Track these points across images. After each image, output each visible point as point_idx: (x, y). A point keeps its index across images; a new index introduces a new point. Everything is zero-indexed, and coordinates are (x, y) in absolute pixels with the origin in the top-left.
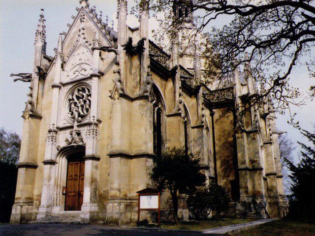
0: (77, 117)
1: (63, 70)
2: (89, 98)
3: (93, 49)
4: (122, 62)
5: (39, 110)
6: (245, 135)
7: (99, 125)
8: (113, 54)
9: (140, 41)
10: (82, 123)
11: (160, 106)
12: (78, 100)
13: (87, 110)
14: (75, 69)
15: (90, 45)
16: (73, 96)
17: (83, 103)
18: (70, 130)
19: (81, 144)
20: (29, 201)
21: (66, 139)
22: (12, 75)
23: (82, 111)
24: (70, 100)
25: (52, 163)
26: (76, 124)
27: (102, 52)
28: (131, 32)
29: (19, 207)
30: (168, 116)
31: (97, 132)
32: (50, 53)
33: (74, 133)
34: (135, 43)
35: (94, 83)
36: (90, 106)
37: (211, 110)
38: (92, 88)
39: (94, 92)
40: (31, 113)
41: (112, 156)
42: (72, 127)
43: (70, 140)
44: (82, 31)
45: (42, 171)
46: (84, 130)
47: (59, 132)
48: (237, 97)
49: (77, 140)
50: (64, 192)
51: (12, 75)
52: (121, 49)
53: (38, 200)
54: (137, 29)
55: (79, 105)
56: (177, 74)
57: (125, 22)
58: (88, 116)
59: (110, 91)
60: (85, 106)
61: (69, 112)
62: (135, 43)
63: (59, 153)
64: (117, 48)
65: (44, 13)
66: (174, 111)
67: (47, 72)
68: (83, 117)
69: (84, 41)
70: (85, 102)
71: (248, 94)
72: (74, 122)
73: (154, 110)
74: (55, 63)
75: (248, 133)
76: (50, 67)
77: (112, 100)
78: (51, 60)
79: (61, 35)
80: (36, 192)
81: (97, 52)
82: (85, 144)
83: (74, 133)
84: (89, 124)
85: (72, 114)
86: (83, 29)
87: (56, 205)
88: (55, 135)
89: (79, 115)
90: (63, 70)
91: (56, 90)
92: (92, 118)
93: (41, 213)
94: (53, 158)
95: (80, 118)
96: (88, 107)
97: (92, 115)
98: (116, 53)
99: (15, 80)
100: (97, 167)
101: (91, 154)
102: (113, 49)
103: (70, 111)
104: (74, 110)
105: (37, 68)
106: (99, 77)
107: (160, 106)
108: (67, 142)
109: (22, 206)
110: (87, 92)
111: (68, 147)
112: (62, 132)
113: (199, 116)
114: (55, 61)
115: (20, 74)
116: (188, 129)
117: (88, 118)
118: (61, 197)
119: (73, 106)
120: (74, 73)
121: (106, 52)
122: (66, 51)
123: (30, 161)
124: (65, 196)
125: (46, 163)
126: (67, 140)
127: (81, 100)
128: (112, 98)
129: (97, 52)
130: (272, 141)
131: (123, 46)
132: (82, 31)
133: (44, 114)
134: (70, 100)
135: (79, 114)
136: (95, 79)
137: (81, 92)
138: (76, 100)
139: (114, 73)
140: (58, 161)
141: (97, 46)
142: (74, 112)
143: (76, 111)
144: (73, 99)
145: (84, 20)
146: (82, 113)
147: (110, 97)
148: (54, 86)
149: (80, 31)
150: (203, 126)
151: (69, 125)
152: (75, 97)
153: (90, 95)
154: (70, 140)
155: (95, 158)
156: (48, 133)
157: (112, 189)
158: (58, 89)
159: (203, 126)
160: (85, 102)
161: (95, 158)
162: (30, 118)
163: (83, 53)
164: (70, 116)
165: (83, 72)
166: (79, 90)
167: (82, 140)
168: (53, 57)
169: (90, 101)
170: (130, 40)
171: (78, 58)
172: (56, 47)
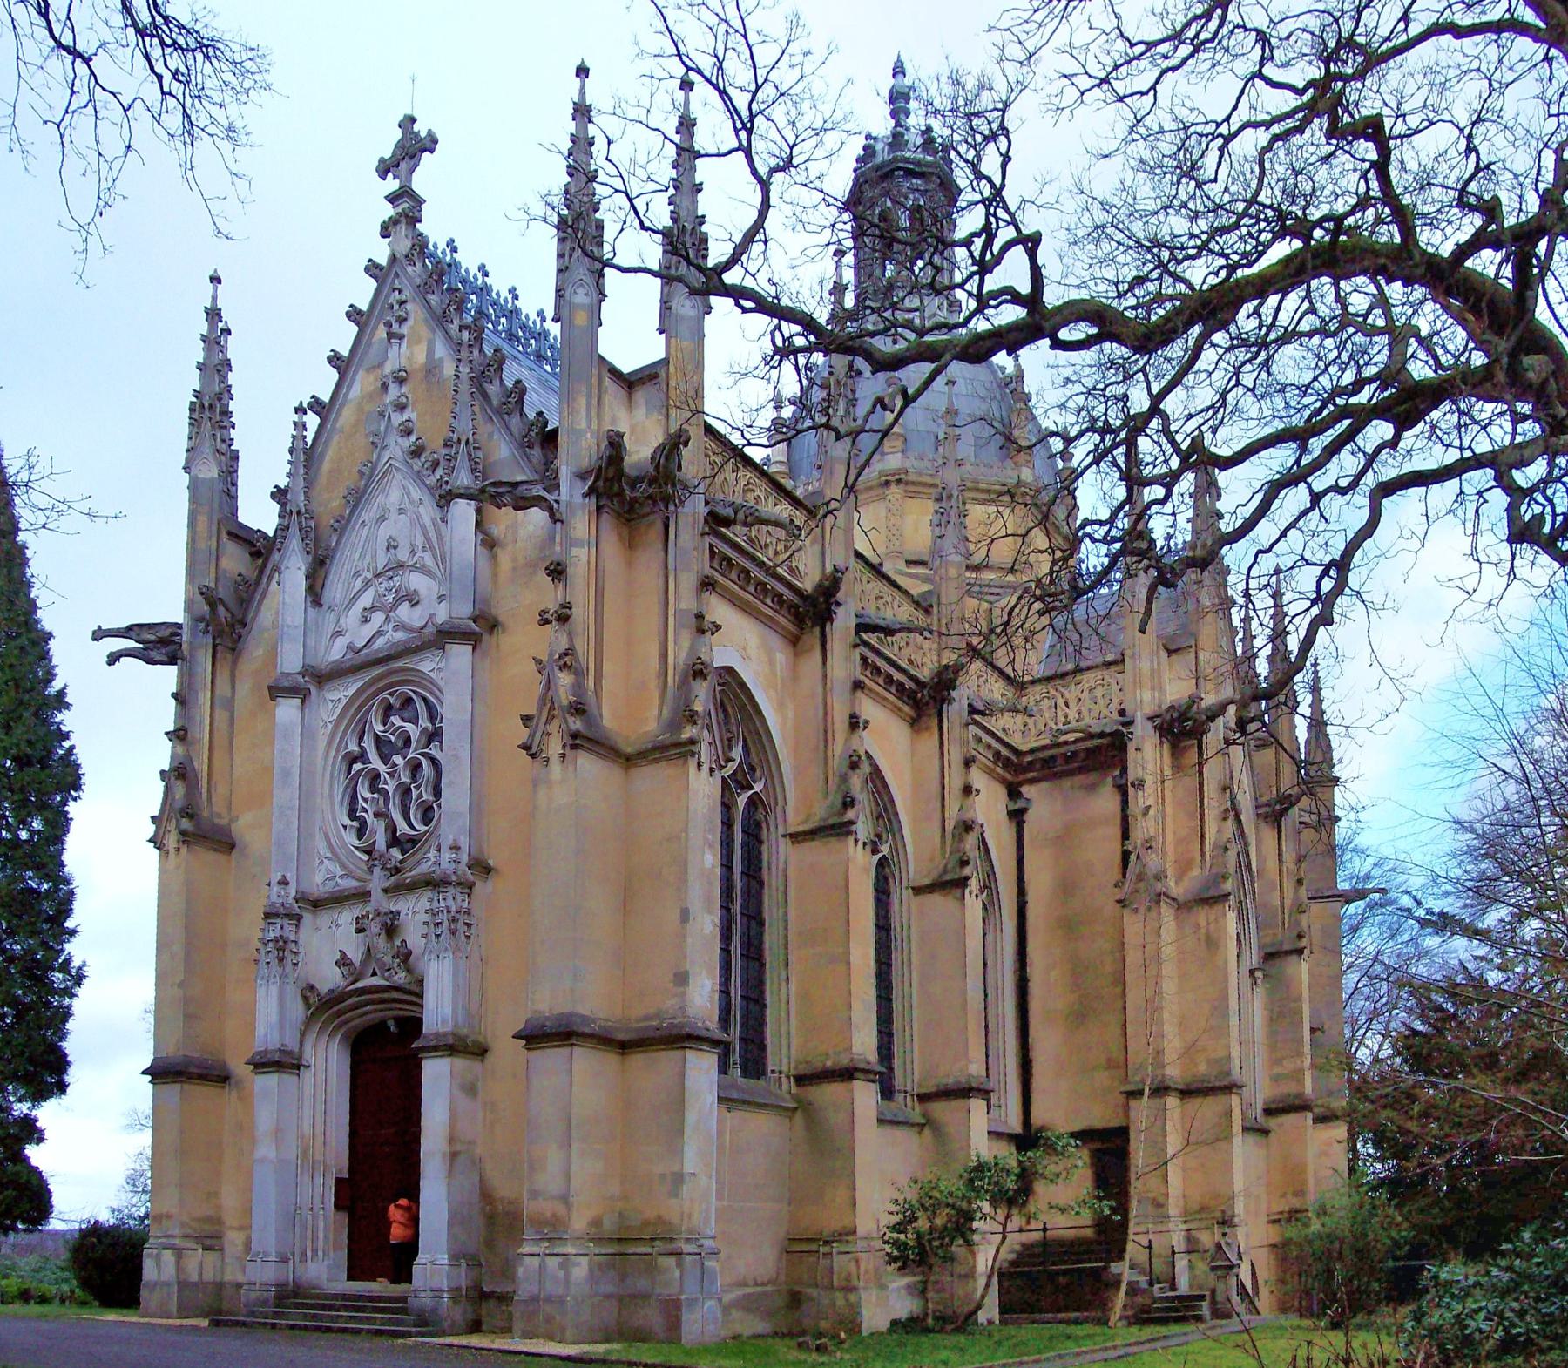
0: (381, 841)
1: (317, 603)
2: (433, 750)
3: (445, 498)
4: (580, 560)
5: (214, 808)
6: (1167, 913)
7: (479, 885)
8: (537, 515)
9: (661, 447)
10: (409, 876)
11: (758, 787)
12: (385, 759)
13: (427, 814)
14: (366, 600)
15: (436, 464)
16: (361, 739)
17: (405, 779)
18: (357, 911)
19: (401, 978)
20: (209, 1229)
21: (338, 956)
22: (99, 635)
25: (284, 1063)
26: (377, 882)
27: (490, 509)
28: (622, 393)
29: (168, 1256)
30: (796, 837)
31: (469, 925)
32: (259, 514)
34: (640, 451)
36: (437, 793)
37: (1013, 792)
38: (447, 699)
39: (455, 710)
40: (186, 824)
41: (536, 1036)
42: (363, 895)
43: (356, 956)
44: (394, 391)
45: (246, 1099)
46: (414, 911)
47: (307, 917)
48: (1139, 718)
49: (388, 959)
51: (99, 635)
52: (570, 491)
53: (241, 1228)
55: (390, 787)
56: (840, 611)
59: (526, 719)
60: (415, 794)
61: (347, 821)
62: (640, 451)
63: (309, 1022)
64: (554, 486)
66: (820, 812)
67: (245, 615)
69: (407, 443)
70: (415, 768)
71: (1194, 700)
72: (370, 870)
73: (727, 807)
74: (277, 569)
75: (1182, 907)
76: (258, 582)
77: (538, 764)
78: (259, 548)
80: (230, 1200)
81: (464, 511)
82: (421, 982)
84: (434, 883)
86: (401, 381)
87: (315, 1252)
88: (292, 937)
89: (394, 840)
90: (317, 603)
91: (287, 710)
92: (447, 855)
94: (292, 1043)
95: (396, 853)
97: (447, 841)
98: (554, 518)
99: (113, 659)
100: (471, 1090)
101: (448, 1028)
102: (537, 491)
103: (352, 814)
105: (199, 598)
106: (470, 638)
107: (758, 787)
108: (346, 970)
109: (178, 1252)
110: (424, 722)
112: (325, 918)
113: (949, 826)
114: (276, 556)
115: (130, 628)
116: (895, 898)
118: (331, 1220)
119: (364, 791)
120: (366, 620)
121: (507, 512)
122: (330, 502)
123: (196, 1055)
125: (264, 1064)
126: (344, 962)
127: (397, 759)
128: (533, 756)
129: (464, 511)
130: (1304, 942)
131: (582, 476)
133: (244, 826)
135: (391, 828)
136: (460, 654)
137: (396, 720)
138: (376, 763)
139: (545, 622)
140: (308, 1055)
141: (463, 479)
142: (370, 819)
143: (377, 815)
144: (362, 757)
145: (405, 330)
146: (402, 827)
147: (526, 747)
148: (277, 691)
149: (385, 387)
151: (349, 884)
152: (369, 744)
153: (434, 736)
154: (356, 956)
155: (455, 1046)
156: (262, 924)
157: (534, 1194)
160: (415, 768)
161: (455, 1046)
162: (184, 849)
164: (351, 839)
165: (404, 611)
166: (388, 711)
169: (434, 762)
170: (615, 444)
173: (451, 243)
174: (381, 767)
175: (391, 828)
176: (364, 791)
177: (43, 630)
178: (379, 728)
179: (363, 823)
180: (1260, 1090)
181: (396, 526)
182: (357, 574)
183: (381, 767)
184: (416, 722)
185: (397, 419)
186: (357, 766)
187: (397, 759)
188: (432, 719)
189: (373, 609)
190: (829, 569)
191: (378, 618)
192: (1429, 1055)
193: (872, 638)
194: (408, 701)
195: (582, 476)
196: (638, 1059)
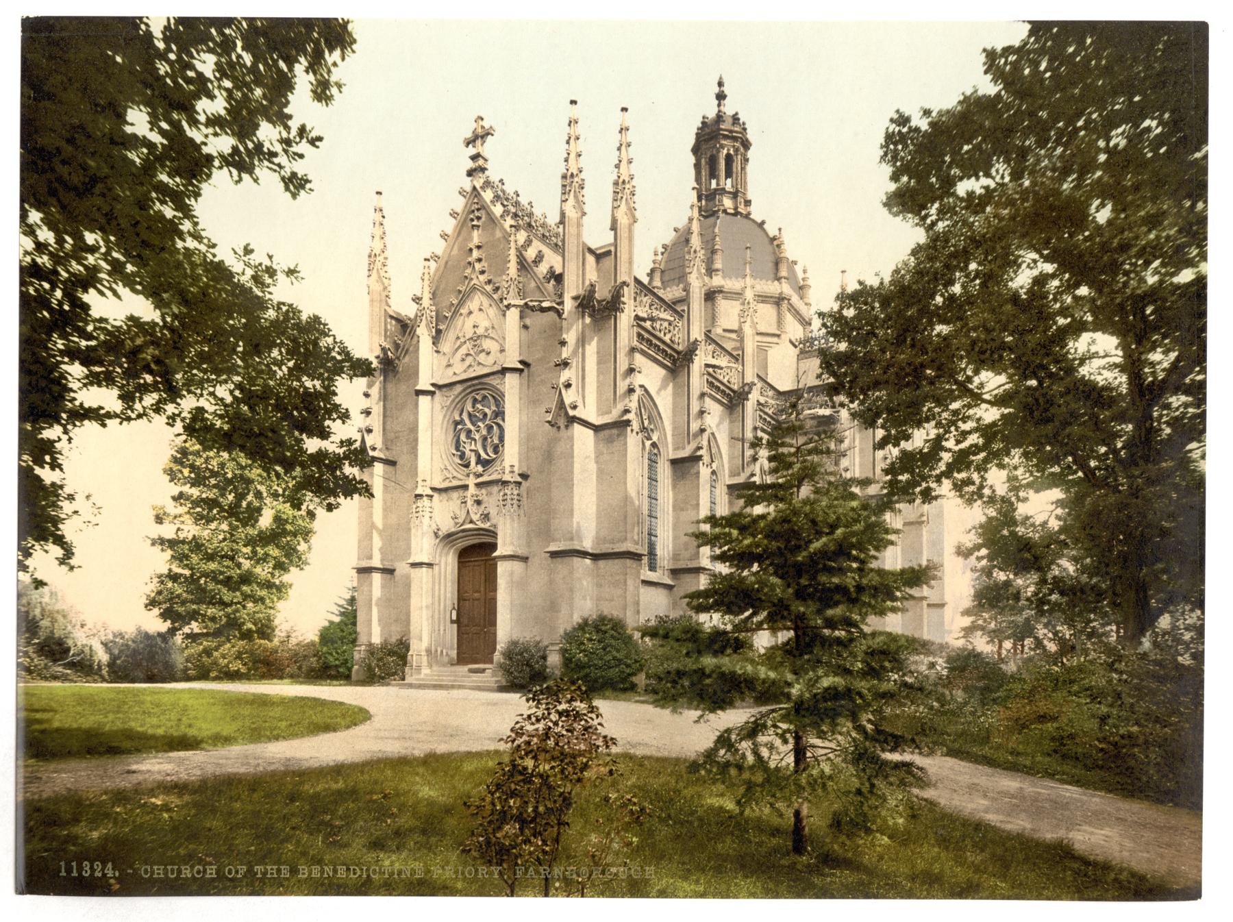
12: (473, 424)
13: (496, 449)
14: (463, 350)
17: (484, 432)
23: (485, 451)
24: (456, 423)
33: (470, 503)
35: (511, 386)
50: (454, 617)
54: (608, 253)
55: (477, 437)
57: (579, 235)
58: (498, 463)
65: (382, 202)
68: (486, 463)
79: (427, 263)
83: (470, 503)
85: (462, 456)
93: (181, 227)
95: (480, 469)
96: (496, 441)
97: (507, 464)
103: (457, 449)
104: (468, 447)
110: (494, 408)
111: (457, 533)
117: (497, 466)
119: (463, 437)
124: (455, 626)
127: (480, 424)
132: (476, 254)
134: (456, 423)
137: (479, 406)
138: (469, 426)
142: (468, 452)
144: (462, 422)
146: (483, 455)
150: (628, 423)
152: (465, 416)
158: (429, 397)
159: (628, 423)
160: (490, 428)
163: (480, 310)
166: (475, 401)
167: (486, 517)
168: (412, 316)
171: (469, 322)
172: (419, 295)
173: (530, 203)
174: (472, 428)
175: (479, 456)
176: (463, 437)
177: (1057, 486)
178: (471, 410)
179: (464, 453)
180: (925, 603)
181: (477, 318)
182: (458, 338)
183: (472, 428)
184: (489, 408)
185: (478, 266)
186: (460, 427)
187: (480, 424)
188: (497, 406)
189: (468, 355)
190: (587, 283)
191: (469, 360)
192: (865, 394)
193: (711, 370)
194: (485, 397)
195: (575, 298)
196: (602, 563)
